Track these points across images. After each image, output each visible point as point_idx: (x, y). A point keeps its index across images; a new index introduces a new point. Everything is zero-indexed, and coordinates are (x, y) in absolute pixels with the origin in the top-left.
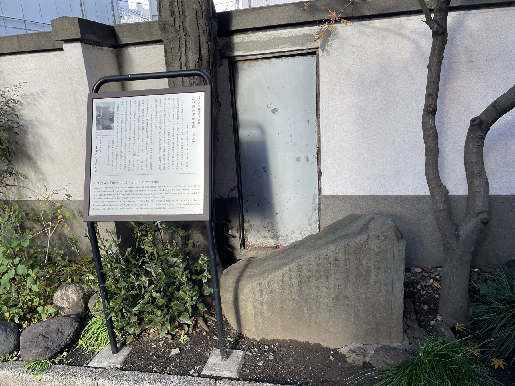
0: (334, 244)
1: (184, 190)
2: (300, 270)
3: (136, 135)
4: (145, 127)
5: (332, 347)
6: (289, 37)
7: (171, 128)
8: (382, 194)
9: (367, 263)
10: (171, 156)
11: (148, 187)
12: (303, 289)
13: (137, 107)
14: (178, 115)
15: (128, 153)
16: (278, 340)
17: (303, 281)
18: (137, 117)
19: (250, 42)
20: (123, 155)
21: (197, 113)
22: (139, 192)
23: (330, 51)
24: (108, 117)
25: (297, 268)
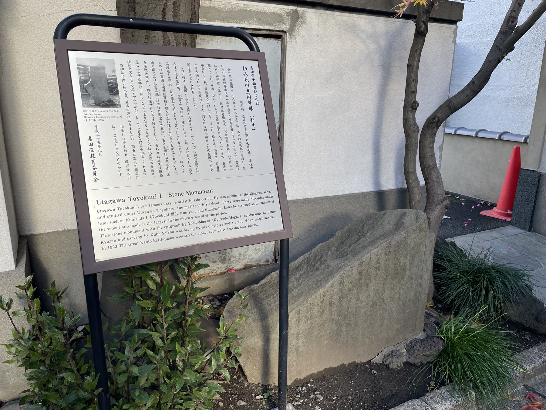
0: (375, 246)
1: (252, 199)
2: (342, 283)
3: (164, 118)
4: (177, 106)
5: (365, 360)
6: (257, 13)
7: (219, 108)
8: (335, 194)
9: (404, 260)
10: (225, 151)
11: (198, 200)
12: (344, 305)
13: (157, 72)
14: (226, 90)
15: (154, 148)
16: (312, 375)
17: (344, 296)
18: (160, 88)
19: (210, 7)
20: (145, 150)
21: (252, 90)
22: (184, 210)
23: (297, 37)
24: (106, 86)
25: (339, 282)
